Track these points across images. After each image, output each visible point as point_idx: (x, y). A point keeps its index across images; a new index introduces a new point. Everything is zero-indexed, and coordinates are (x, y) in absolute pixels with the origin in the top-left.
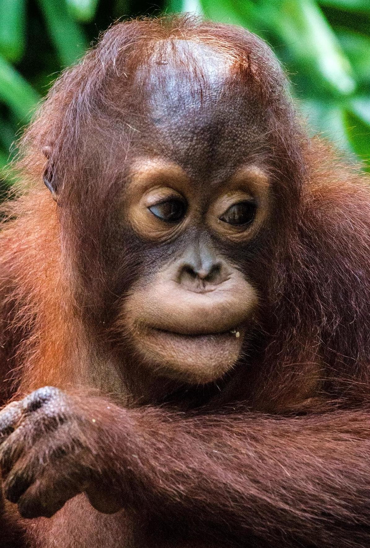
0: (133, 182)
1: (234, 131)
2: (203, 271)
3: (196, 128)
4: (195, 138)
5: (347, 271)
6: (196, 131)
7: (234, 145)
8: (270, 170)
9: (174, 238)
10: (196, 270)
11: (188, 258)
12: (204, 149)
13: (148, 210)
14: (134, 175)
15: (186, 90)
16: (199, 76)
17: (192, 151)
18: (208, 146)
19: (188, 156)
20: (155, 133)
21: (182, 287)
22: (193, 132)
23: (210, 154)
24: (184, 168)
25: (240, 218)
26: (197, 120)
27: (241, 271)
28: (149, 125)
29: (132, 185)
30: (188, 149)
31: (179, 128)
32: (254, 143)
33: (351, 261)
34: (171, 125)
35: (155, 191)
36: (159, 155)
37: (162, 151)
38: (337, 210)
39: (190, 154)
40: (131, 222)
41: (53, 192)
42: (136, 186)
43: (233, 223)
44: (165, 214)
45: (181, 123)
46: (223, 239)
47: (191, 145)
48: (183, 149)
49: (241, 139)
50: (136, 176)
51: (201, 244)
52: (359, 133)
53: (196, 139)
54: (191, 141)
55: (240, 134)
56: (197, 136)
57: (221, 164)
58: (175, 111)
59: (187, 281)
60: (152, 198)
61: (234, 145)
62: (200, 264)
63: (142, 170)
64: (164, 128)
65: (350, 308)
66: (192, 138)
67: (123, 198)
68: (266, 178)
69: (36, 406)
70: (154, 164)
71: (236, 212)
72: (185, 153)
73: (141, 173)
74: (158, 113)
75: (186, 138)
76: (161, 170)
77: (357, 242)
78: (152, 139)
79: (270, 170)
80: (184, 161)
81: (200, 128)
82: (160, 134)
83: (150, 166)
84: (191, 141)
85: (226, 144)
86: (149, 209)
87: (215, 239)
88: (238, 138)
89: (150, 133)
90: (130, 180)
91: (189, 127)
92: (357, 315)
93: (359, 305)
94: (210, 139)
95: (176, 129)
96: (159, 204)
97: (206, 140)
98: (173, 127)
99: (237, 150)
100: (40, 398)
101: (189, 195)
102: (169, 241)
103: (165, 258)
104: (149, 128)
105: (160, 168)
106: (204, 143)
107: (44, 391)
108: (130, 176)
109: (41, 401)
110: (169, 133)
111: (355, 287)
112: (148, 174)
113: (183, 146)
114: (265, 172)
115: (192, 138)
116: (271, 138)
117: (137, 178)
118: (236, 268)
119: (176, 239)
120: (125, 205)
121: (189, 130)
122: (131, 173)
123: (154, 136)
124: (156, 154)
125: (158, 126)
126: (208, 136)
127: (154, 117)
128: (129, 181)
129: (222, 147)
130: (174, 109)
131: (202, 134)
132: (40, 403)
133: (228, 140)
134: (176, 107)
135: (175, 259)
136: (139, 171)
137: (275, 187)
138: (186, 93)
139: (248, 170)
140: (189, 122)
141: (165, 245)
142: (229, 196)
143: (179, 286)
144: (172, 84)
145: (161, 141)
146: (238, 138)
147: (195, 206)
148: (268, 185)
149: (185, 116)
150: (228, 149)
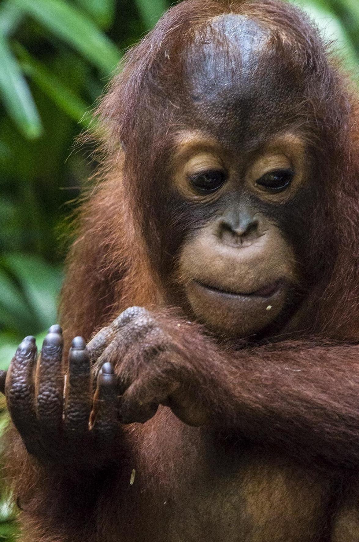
0: (176, 154)
2: (239, 230)
3: (229, 104)
8: (306, 135)
9: (216, 199)
11: (228, 218)
12: (236, 123)
17: (225, 125)
18: (240, 120)
21: (222, 242)
22: (227, 109)
23: (242, 127)
27: (278, 227)
29: (177, 155)
31: (214, 104)
32: (287, 114)
40: (178, 187)
45: (216, 100)
48: (217, 124)
50: (178, 148)
57: (254, 134)
58: (211, 89)
59: (227, 236)
62: (238, 224)
69: (127, 320)
72: (220, 127)
73: (183, 145)
74: (198, 91)
75: (220, 113)
79: (306, 135)
81: (232, 105)
85: (258, 117)
87: (255, 200)
90: (174, 151)
95: (211, 106)
98: (209, 104)
100: (129, 314)
102: (211, 202)
103: (207, 217)
105: (199, 140)
106: (236, 118)
107: (131, 310)
108: (173, 148)
109: (130, 316)
113: (217, 121)
114: (300, 138)
115: (226, 113)
117: (179, 150)
118: (274, 225)
120: (172, 172)
121: (223, 106)
122: (175, 144)
125: (196, 104)
126: (240, 111)
128: (174, 152)
131: (234, 110)
132: (129, 318)
133: (259, 113)
134: (213, 85)
135: (216, 217)
136: (181, 143)
139: (280, 138)
141: (207, 206)
143: (220, 241)
145: (199, 116)
150: (259, 122)
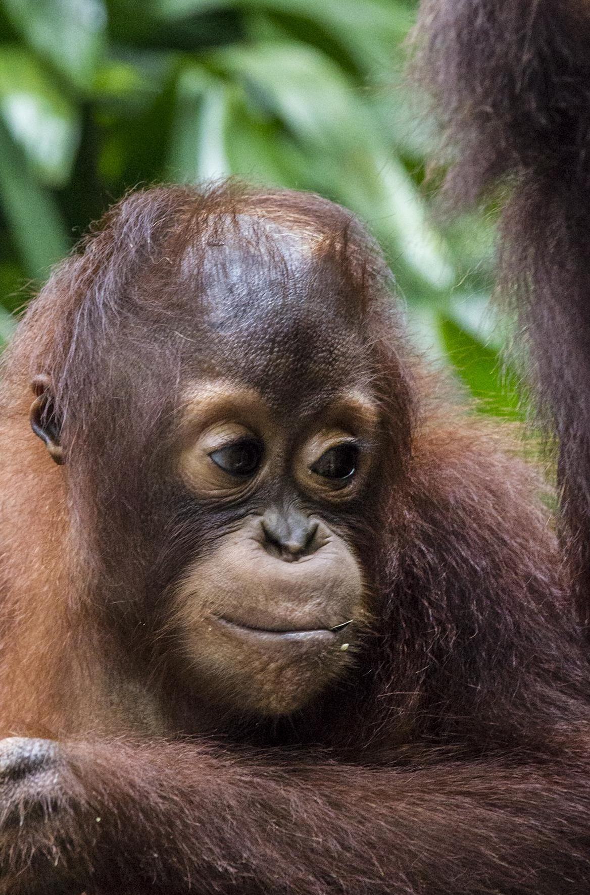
0: (185, 418)
1: (330, 339)
2: (294, 543)
4: (276, 349)
5: (465, 561)
6: (278, 339)
7: (331, 360)
10: (284, 541)
13: (209, 458)
14: (187, 406)
15: (258, 279)
16: (278, 261)
18: (294, 361)
19: (267, 375)
20: (216, 344)
24: (262, 393)
25: (337, 469)
26: (278, 323)
28: (207, 332)
29: (185, 421)
30: (266, 366)
33: (468, 546)
34: (241, 331)
35: (218, 429)
36: (223, 375)
37: (229, 369)
38: (449, 472)
39: (270, 372)
41: (49, 442)
42: (190, 422)
43: (327, 474)
44: (232, 464)
46: (316, 498)
47: (270, 360)
48: (259, 365)
49: (339, 350)
51: (285, 506)
52: (188, 670)
53: (278, 352)
54: (271, 352)
55: (338, 343)
56: (279, 346)
57: (315, 385)
60: (216, 438)
61: (331, 360)
63: (198, 398)
64: (230, 336)
65: (470, 616)
66: (272, 348)
67: (171, 439)
68: (372, 408)
70: (217, 389)
71: (332, 461)
73: (198, 403)
74: (218, 315)
75: (262, 348)
76: (229, 396)
77: (478, 519)
78: (212, 352)
79: (376, 397)
80: (260, 383)
82: (225, 344)
83: (211, 391)
84: (271, 352)
86: (211, 457)
88: (335, 348)
89: (208, 344)
90: (181, 414)
91: (266, 333)
92: (478, 625)
93: (481, 609)
94: (296, 352)
95: (248, 336)
96: (224, 448)
97: (291, 352)
99: (336, 367)
101: (267, 434)
104: (206, 337)
105: (227, 394)
106: (289, 357)
110: (238, 342)
111: (475, 585)
112: (209, 404)
113: (261, 362)
115: (272, 348)
116: (374, 351)
119: (250, 497)
123: (215, 348)
124: (219, 375)
127: (214, 320)
129: (315, 362)
130: (242, 308)
133: (323, 351)
137: (384, 422)
138: (258, 284)
140: (266, 326)
142: (323, 435)
144: (236, 272)
146: (335, 348)
147: (276, 448)
148: (375, 419)
149: (260, 317)
